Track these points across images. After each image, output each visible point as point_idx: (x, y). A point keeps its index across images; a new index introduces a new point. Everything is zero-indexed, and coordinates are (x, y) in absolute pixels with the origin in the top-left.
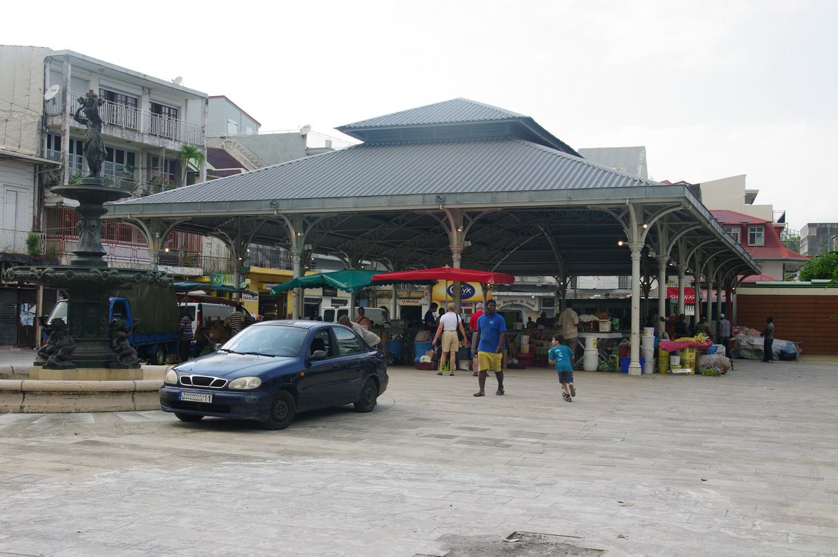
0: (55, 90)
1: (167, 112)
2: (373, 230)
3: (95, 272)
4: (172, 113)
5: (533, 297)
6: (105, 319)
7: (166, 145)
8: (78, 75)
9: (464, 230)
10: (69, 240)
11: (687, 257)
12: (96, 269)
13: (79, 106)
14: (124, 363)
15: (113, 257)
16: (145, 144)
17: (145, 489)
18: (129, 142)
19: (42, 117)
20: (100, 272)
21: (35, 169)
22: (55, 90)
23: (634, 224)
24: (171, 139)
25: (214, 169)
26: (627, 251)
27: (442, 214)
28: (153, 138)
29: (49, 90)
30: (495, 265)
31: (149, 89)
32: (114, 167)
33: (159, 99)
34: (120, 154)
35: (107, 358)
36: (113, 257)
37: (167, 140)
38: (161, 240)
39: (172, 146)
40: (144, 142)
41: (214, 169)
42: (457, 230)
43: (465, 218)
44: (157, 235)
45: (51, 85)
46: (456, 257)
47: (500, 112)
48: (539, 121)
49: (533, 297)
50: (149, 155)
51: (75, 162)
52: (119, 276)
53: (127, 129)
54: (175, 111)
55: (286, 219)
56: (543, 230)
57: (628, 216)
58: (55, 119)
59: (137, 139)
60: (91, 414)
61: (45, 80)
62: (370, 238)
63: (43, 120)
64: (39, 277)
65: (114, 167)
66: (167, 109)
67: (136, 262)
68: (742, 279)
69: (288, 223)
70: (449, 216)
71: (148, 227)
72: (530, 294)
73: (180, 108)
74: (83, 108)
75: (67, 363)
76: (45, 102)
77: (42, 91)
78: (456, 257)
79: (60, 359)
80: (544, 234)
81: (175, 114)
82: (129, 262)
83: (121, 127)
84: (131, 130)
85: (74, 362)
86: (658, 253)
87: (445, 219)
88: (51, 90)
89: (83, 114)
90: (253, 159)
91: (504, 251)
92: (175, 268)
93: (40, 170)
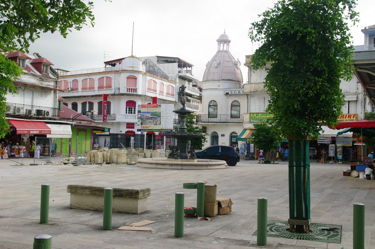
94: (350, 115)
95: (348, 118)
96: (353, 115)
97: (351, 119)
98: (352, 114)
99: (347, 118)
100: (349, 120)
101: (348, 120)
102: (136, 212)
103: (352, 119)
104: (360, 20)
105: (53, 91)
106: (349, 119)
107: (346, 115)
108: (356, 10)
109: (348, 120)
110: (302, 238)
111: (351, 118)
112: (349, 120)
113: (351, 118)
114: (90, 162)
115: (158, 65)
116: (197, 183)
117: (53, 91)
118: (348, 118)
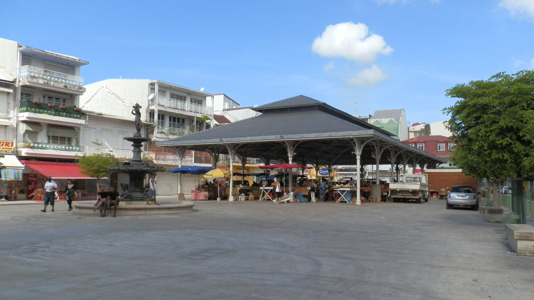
0: (152, 96)
2: (274, 148)
3: (136, 167)
4: (200, 102)
5: (354, 174)
8: (161, 89)
9: (293, 148)
11: (395, 157)
12: (136, 166)
17: (64, 244)
21: (145, 127)
22: (152, 96)
23: (289, 148)
24: (192, 112)
25: (218, 124)
26: (355, 156)
27: (284, 142)
30: (332, 161)
31: (190, 93)
32: (176, 125)
33: (193, 97)
34: (179, 119)
35: (143, 197)
37: (197, 113)
39: (199, 115)
41: (218, 124)
42: (290, 148)
43: (234, 146)
46: (290, 159)
47: (314, 100)
48: (328, 103)
49: (354, 174)
55: (227, 146)
56: (351, 146)
57: (354, 143)
59: (185, 113)
62: (250, 147)
66: (194, 100)
68: (438, 166)
69: (228, 147)
70: (287, 144)
72: (353, 173)
73: (203, 100)
77: (148, 96)
78: (290, 159)
79: (126, 198)
80: (351, 148)
84: (182, 110)
86: (375, 156)
87: (353, 142)
90: (235, 119)
91: (336, 154)
92: (201, 164)
94: (8, 142)
95: (6, 146)
96: (11, 143)
97: (8, 148)
98: (10, 142)
99: (4, 146)
100: (6, 148)
101: (5, 149)
102: (51, 129)
103: (10, 147)
104: (446, 129)
105: (436, 193)
106: (7, 147)
107: (3, 142)
108: (447, 129)
109: (5, 149)
110: (231, 116)
111: (9, 146)
112: (6, 148)
113: (9, 146)
114: (97, 150)
115: (390, 119)
116: (420, 130)
117: (436, 193)
118: (6, 146)
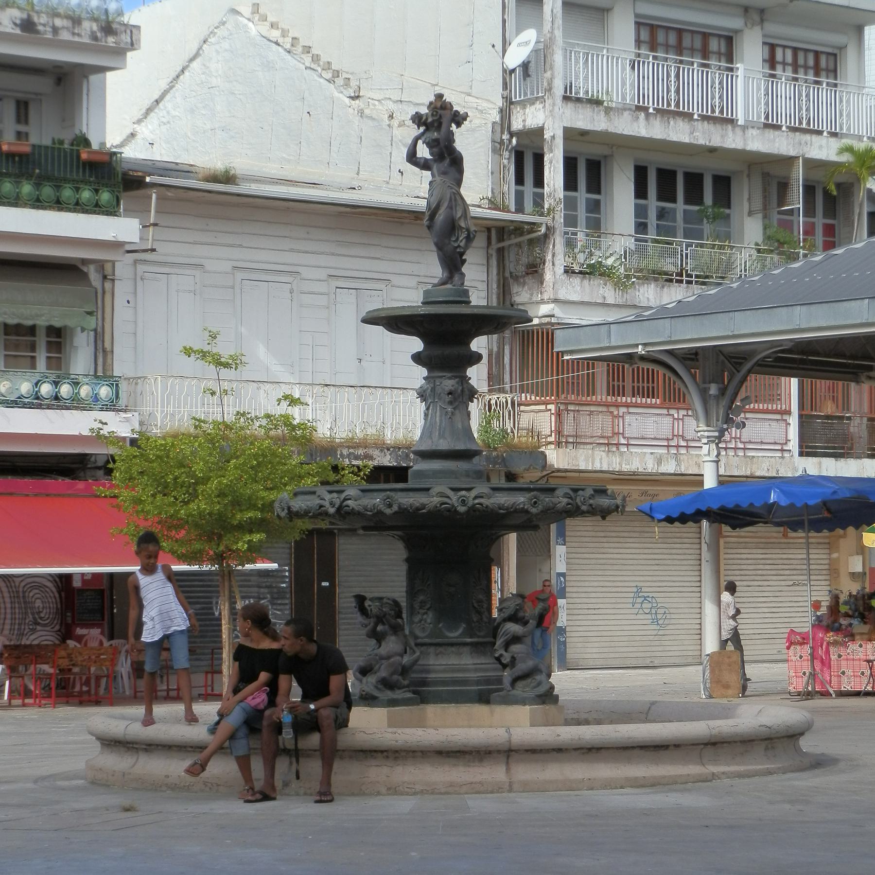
1: (811, 62)
6: (481, 597)
7: (806, 149)
10: (571, 407)
13: (414, 131)
14: (520, 690)
15: (683, 443)
16: (751, 153)
18: (712, 150)
19: (501, 111)
20: (451, 493)
21: (489, 239)
22: (527, 43)
28: (771, 134)
29: (514, 44)
31: (762, 11)
32: (680, 216)
34: (694, 181)
35: (488, 681)
36: (683, 443)
37: (807, 137)
38: (724, 402)
40: (748, 148)
44: (713, 390)
45: (519, 31)
50: (766, 176)
51: (582, 214)
52: (492, 501)
53: (704, 118)
54: (832, 58)
58: (530, 110)
59: (732, 140)
60: (334, 778)
61: (504, 21)
63: (502, 118)
64: (332, 510)
65: (680, 216)
66: (789, 54)
67: (741, 453)
71: (688, 369)
73: (842, 48)
74: (423, 134)
75: (398, 694)
76: (508, 73)
77: (499, 47)
79: (387, 684)
81: (831, 66)
82: (663, 451)
83: (688, 116)
85: (414, 692)
88: (519, 45)
89: (423, 151)
92: (842, 462)
93: (501, 239)
